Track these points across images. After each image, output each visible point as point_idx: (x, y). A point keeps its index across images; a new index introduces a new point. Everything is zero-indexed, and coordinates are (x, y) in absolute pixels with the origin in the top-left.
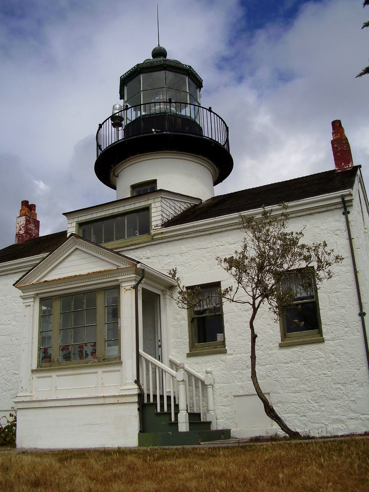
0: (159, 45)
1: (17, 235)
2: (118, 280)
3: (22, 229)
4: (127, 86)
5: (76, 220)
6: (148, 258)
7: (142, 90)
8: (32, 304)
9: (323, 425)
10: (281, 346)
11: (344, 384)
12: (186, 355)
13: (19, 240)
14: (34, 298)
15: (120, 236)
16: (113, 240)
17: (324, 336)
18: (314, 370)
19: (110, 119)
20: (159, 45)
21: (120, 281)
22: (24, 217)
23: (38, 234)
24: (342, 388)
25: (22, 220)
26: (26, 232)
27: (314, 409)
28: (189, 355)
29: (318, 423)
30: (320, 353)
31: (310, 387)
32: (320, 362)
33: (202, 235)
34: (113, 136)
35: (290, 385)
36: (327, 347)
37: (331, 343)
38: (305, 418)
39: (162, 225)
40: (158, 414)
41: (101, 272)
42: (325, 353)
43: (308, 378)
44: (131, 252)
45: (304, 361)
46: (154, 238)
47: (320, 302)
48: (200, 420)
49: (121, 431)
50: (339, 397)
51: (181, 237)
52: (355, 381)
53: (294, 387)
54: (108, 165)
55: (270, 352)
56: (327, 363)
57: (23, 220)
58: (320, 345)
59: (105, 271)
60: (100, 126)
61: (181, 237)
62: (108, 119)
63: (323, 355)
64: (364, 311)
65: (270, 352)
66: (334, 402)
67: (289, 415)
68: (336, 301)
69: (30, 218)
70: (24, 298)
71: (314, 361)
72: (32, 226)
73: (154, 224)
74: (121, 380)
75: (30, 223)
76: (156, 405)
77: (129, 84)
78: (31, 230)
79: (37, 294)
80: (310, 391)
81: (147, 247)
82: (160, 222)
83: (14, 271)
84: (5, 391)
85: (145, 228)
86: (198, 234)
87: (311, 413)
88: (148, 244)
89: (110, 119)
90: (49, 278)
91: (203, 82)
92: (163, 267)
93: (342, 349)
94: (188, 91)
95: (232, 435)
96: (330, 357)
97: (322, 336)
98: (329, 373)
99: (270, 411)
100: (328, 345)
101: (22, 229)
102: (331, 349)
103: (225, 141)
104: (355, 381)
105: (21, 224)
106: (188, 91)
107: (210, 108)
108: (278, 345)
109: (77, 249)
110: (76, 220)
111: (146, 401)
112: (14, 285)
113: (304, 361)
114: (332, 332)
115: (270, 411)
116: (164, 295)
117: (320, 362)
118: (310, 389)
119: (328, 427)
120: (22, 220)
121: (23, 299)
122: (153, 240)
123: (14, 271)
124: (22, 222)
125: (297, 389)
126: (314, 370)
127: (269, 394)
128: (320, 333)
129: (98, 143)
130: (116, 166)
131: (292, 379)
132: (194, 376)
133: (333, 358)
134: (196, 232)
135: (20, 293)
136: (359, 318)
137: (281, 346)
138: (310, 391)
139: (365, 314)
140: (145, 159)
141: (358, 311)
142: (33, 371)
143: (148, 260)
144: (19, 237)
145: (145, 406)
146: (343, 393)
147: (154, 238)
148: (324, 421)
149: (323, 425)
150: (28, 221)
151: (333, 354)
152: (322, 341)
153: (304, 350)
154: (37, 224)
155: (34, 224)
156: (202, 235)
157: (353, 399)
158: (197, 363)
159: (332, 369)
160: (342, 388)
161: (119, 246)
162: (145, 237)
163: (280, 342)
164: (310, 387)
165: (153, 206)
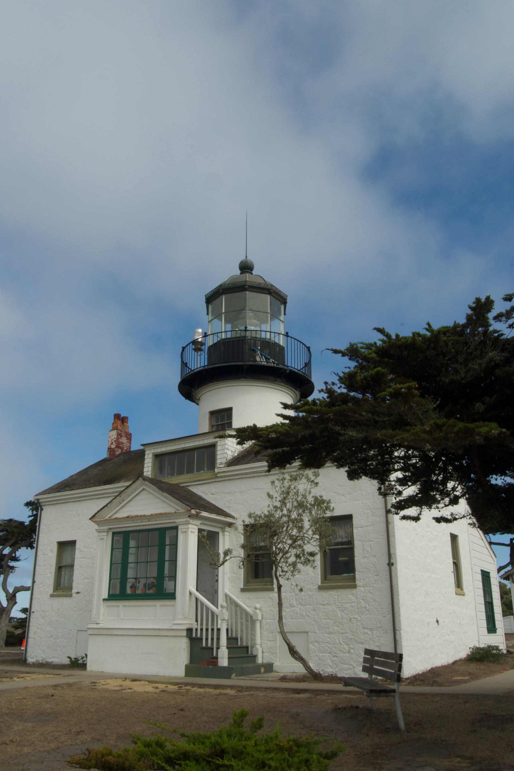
0: (246, 257)
1: (109, 448)
2: (174, 522)
3: (114, 443)
4: (211, 304)
5: (153, 451)
6: (213, 494)
7: (223, 311)
8: (105, 537)
9: (351, 667)
10: (320, 588)
11: (371, 630)
12: (240, 590)
13: (110, 454)
14: (107, 532)
15: (190, 471)
16: (183, 473)
17: (357, 582)
18: (347, 614)
19: (191, 344)
20: (246, 257)
21: (177, 523)
22: (115, 431)
23: (130, 447)
24: (369, 633)
25: (114, 434)
26: (118, 447)
27: (344, 650)
28: (243, 590)
29: (347, 664)
30: (352, 598)
31: (342, 629)
32: (352, 606)
33: (259, 476)
34: (199, 362)
35: (325, 626)
36: (359, 593)
37: (362, 589)
38: (336, 658)
39: (226, 463)
40: (203, 648)
41: (161, 514)
42: (357, 599)
43: (341, 620)
44: (199, 487)
45: (339, 604)
46: (218, 475)
47: (355, 550)
48: (248, 653)
49: (172, 661)
50: (366, 641)
51: (241, 476)
52: (381, 627)
53: (329, 628)
54: (192, 385)
55: (310, 593)
56: (358, 608)
57: (114, 433)
58: (354, 591)
59: (165, 514)
60: (184, 348)
61: (241, 476)
62: (189, 344)
63: (355, 600)
64: (392, 561)
65: (310, 593)
66: (361, 646)
67: (323, 654)
68: (369, 549)
69: (121, 431)
70: (99, 531)
71: (347, 605)
72: (124, 440)
73: (218, 461)
74: (179, 613)
75: (121, 436)
76: (202, 639)
77: (214, 302)
78: (122, 443)
79: (110, 529)
80: (342, 633)
81: (212, 484)
82: (224, 461)
83: (98, 497)
84: (86, 612)
85: (212, 464)
86: (256, 475)
87: (342, 655)
88: (213, 480)
89: (191, 344)
90: (120, 515)
91: (288, 298)
92: (225, 504)
93: (371, 596)
94: (269, 312)
95: (274, 669)
96: (360, 602)
97: (355, 582)
98: (359, 618)
99: (293, 652)
100: (360, 590)
101: (114, 443)
102: (362, 595)
103: (181, 485)
104: (381, 627)
105: (113, 438)
106: (269, 312)
107: (287, 333)
108: (317, 587)
109: (144, 489)
110: (153, 451)
111: (194, 635)
112: (90, 519)
113: (339, 604)
114: (364, 579)
115: (293, 652)
116: (223, 531)
117: (352, 606)
118: (342, 631)
119: (355, 669)
120: (114, 434)
121: (98, 532)
122: (217, 477)
123: (98, 497)
124: (114, 436)
125: (331, 630)
126: (347, 614)
127: (307, 632)
128: (354, 579)
129: (182, 361)
130: (197, 391)
131: (327, 621)
132: (245, 611)
133: (363, 604)
134: (254, 472)
135: (96, 527)
136: (387, 568)
137: (320, 588)
138: (342, 633)
139: (392, 564)
140: (223, 386)
141: (387, 561)
142: (104, 600)
143: (213, 496)
144: (110, 452)
145: (193, 639)
146: (370, 638)
147: (218, 475)
148: (352, 663)
149: (351, 667)
150: (119, 435)
151: (363, 600)
152: (355, 587)
153: (339, 594)
154: (129, 437)
155: (126, 437)
156: (259, 476)
157: (378, 644)
158: (249, 598)
159: (362, 614)
160: (369, 633)
161: (188, 480)
162: (209, 474)
163: (320, 584)
164: (342, 629)
165: (219, 444)
